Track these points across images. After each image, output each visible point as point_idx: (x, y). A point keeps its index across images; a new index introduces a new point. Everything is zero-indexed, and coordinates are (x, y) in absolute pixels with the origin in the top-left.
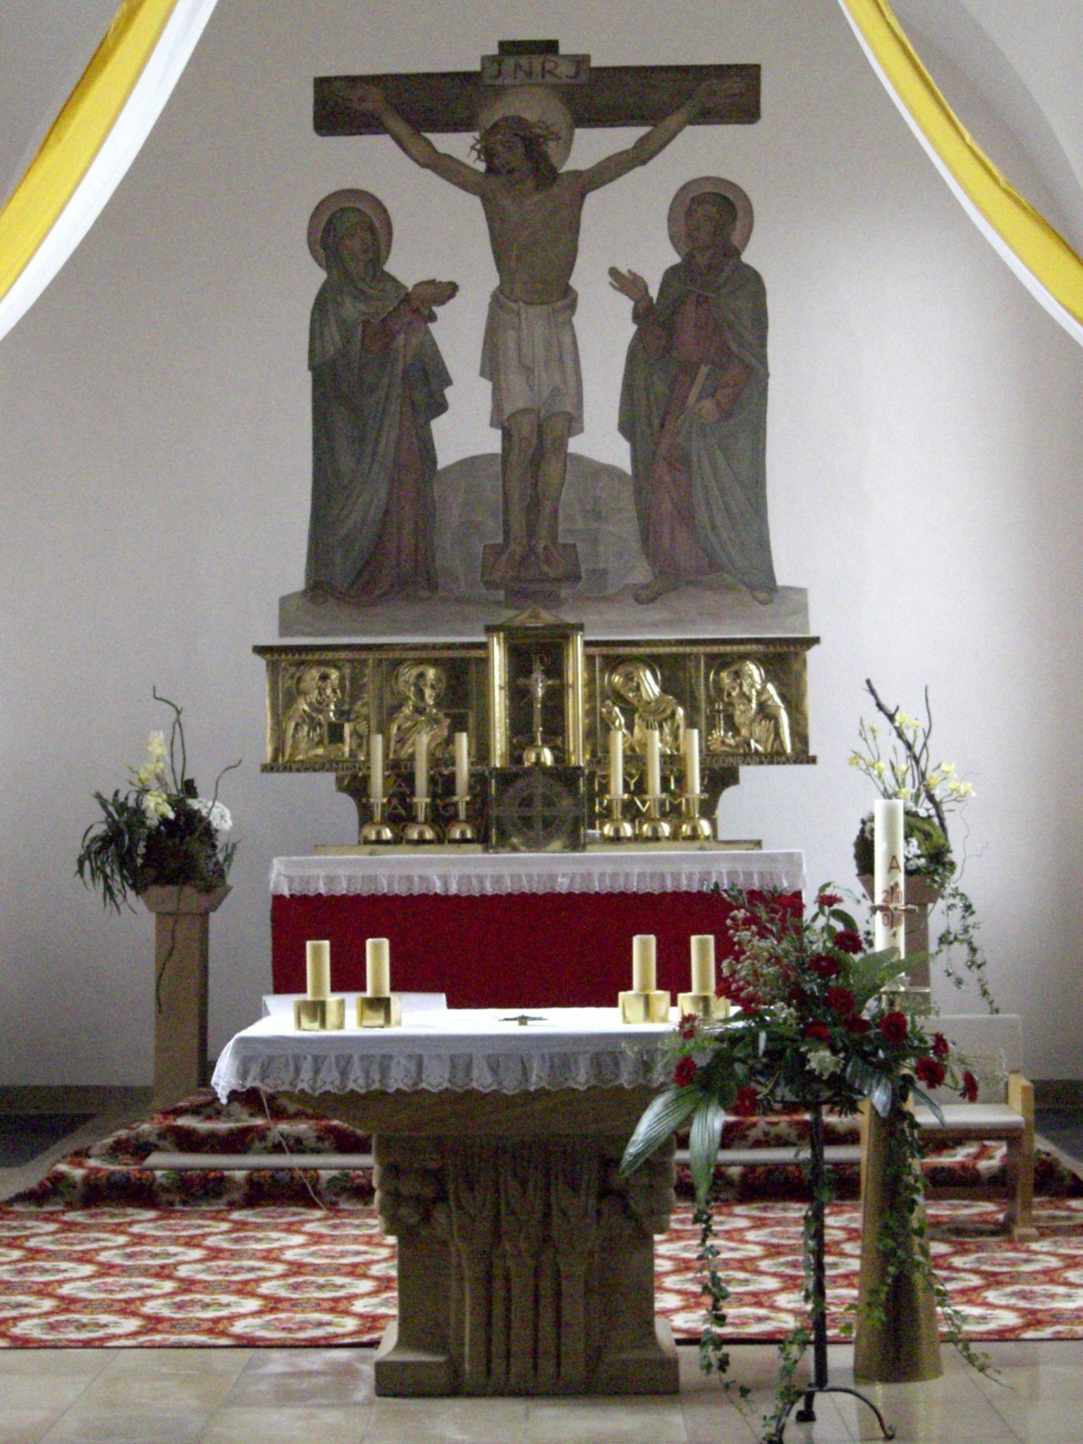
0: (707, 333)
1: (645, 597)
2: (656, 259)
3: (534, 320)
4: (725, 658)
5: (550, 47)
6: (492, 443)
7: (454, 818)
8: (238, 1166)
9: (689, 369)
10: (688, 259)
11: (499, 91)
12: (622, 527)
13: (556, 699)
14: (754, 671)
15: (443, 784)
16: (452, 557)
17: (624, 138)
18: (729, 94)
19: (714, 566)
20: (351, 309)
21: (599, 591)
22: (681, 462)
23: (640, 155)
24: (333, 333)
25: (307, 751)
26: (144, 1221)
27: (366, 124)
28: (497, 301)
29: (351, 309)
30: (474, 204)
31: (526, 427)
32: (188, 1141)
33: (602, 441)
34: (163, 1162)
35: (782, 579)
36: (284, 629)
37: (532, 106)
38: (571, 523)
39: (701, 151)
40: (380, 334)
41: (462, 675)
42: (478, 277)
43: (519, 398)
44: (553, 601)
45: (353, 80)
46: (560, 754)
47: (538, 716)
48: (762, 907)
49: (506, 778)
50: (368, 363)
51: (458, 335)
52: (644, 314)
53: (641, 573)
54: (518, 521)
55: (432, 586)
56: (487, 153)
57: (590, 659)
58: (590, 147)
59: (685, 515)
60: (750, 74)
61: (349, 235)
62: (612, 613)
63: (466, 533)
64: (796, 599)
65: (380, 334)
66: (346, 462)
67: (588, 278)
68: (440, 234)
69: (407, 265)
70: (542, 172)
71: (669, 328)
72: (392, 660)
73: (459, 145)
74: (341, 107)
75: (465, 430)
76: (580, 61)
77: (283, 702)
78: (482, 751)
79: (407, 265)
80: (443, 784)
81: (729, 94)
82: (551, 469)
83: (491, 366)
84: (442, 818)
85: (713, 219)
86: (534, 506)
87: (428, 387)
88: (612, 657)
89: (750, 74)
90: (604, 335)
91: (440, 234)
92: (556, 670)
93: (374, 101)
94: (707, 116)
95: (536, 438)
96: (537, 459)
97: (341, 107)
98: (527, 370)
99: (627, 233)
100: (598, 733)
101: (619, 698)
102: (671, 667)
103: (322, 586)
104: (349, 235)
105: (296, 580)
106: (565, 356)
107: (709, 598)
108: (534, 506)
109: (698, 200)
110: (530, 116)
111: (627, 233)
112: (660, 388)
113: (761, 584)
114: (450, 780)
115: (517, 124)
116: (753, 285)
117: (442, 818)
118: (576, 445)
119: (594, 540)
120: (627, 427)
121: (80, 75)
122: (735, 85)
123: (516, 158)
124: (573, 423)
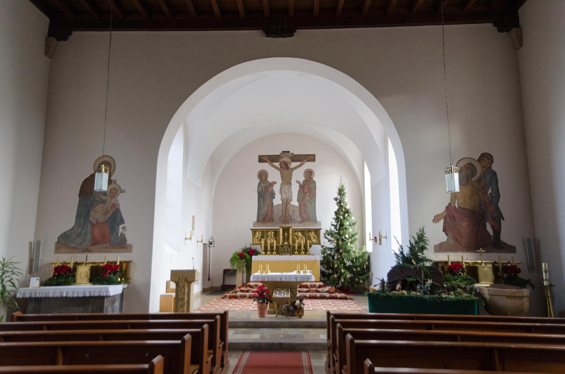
0: (308, 188)
1: (300, 222)
2: (302, 179)
3: (286, 187)
4: (309, 231)
5: (289, 152)
6: (281, 202)
7: (273, 251)
8: (248, 294)
9: (306, 193)
10: (306, 179)
11: (282, 157)
12: (297, 213)
13: (288, 235)
14: (313, 232)
15: (272, 247)
16: (275, 217)
17: (298, 163)
18: (311, 158)
19: (309, 219)
20: (263, 185)
21: (294, 222)
22: (305, 205)
23: (300, 166)
24: (260, 188)
25: (399, 290)
26: (237, 300)
27: (266, 161)
28: (281, 184)
29: (263, 185)
30: (279, 172)
31: (285, 201)
32: (242, 291)
33: (295, 202)
34: (239, 294)
35: (318, 220)
36: (254, 226)
37: (286, 159)
38: (291, 212)
39: (308, 165)
40: (267, 188)
41: (276, 233)
42: (279, 181)
43: (284, 196)
44: (288, 223)
45: (263, 156)
46: (289, 243)
47: (286, 239)
48: (105, 176)
49: (282, 246)
50: (265, 192)
51: (276, 189)
52: (300, 186)
53: (300, 219)
54: (284, 212)
55: (273, 221)
56: (280, 165)
57: (293, 231)
58: (294, 165)
59: (305, 212)
60: (314, 155)
61: (263, 175)
62: (296, 225)
63: (277, 214)
64: (320, 223)
65: (267, 188)
66: (262, 205)
67: (293, 181)
68: (274, 175)
69: (270, 180)
70: (288, 168)
71: (303, 188)
72: (268, 231)
73: (277, 164)
74: (261, 159)
75: (277, 201)
76: (292, 154)
77: (254, 236)
78: (278, 242)
79: (270, 180)
80: (272, 247)
81: (311, 158)
82: (288, 206)
83: (281, 193)
84: (272, 251)
85: (309, 174)
86: (286, 211)
87: (273, 195)
88: (295, 231)
89: (314, 155)
90: (295, 189)
91: (274, 175)
92: (288, 232)
93: (266, 159)
94: (308, 161)
95: (286, 202)
96: (286, 205)
97: (261, 159)
98: (285, 193)
99: (298, 176)
100: (294, 242)
101: (296, 236)
102: (303, 231)
103: (258, 221)
104: (263, 175)
105: (255, 220)
106: (290, 191)
107: (309, 223)
108: (286, 211)
109: (307, 172)
110: (286, 160)
111: (298, 176)
112: (302, 195)
113: (315, 221)
114: (273, 246)
115: (284, 161)
116: (314, 182)
117: (272, 251)
118: (291, 203)
119: (293, 215)
120: (298, 201)
121: (315, 301)
122: (312, 157)
123: (284, 166)
124: (291, 200)
